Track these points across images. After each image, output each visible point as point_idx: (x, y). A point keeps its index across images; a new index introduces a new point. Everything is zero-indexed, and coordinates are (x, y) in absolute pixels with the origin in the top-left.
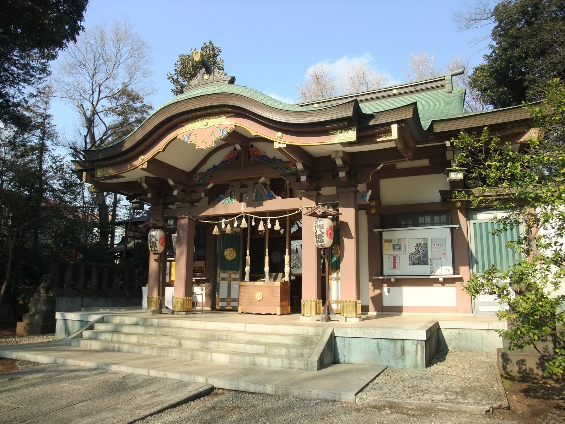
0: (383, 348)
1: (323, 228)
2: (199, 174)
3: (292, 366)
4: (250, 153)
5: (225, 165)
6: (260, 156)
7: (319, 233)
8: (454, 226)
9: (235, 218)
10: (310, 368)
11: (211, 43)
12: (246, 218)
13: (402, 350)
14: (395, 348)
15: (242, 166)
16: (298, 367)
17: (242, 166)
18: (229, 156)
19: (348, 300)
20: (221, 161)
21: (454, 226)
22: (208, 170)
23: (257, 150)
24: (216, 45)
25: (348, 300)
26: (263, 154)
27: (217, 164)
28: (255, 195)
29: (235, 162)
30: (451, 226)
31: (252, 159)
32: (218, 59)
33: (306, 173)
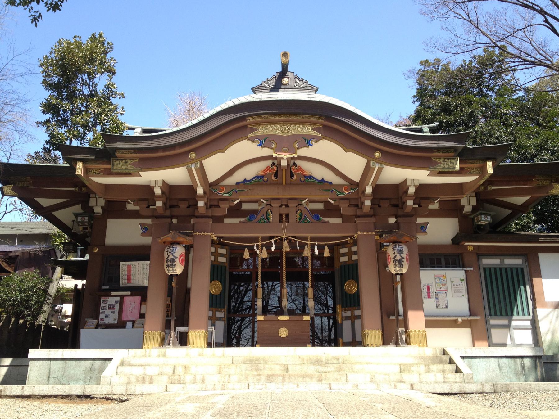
0: (503, 365)
1: (402, 252)
2: (226, 186)
3: (446, 380)
4: (293, 172)
5: (259, 181)
6: (305, 177)
7: (398, 257)
8: (468, 269)
9: (273, 241)
10: (466, 381)
11: (100, 36)
12: (290, 242)
13: (522, 366)
14: (516, 365)
15: (284, 183)
16: (454, 380)
17: (284, 183)
18: (265, 171)
19: (417, 330)
20: (253, 175)
21: (468, 269)
22: (237, 184)
23: (301, 169)
24: (90, 37)
25: (417, 330)
26: (308, 174)
27: (249, 178)
28: (298, 216)
29: (274, 178)
30: (465, 269)
31: (295, 178)
32: (109, 56)
33: (371, 198)
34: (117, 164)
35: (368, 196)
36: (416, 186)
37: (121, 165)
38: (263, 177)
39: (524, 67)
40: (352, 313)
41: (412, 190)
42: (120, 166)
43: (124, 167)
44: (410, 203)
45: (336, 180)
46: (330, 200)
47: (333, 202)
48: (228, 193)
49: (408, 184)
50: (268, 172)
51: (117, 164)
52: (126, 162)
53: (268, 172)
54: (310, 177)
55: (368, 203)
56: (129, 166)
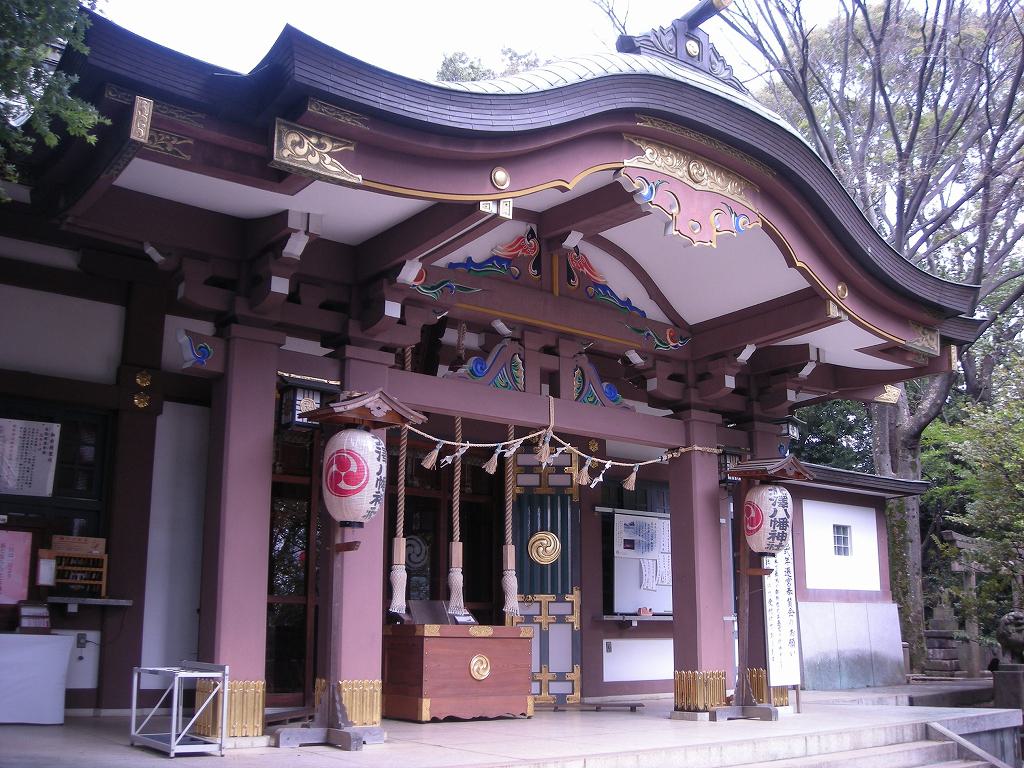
15: (556, 293)
17: (556, 293)
23: (587, 264)
26: (601, 281)
29: (533, 272)
31: (575, 283)
34: (294, 144)
35: (290, 262)
36: (311, 235)
37: (304, 150)
38: (509, 261)
39: (629, 90)
40: (252, 744)
41: (296, 247)
42: (301, 151)
43: (314, 160)
44: (280, 286)
45: (653, 312)
46: (150, 250)
47: (157, 257)
48: (433, 288)
49: (291, 224)
50: (520, 252)
51: (294, 144)
52: (320, 146)
53: (520, 252)
54: (605, 288)
55: (280, 286)
56: (328, 159)
